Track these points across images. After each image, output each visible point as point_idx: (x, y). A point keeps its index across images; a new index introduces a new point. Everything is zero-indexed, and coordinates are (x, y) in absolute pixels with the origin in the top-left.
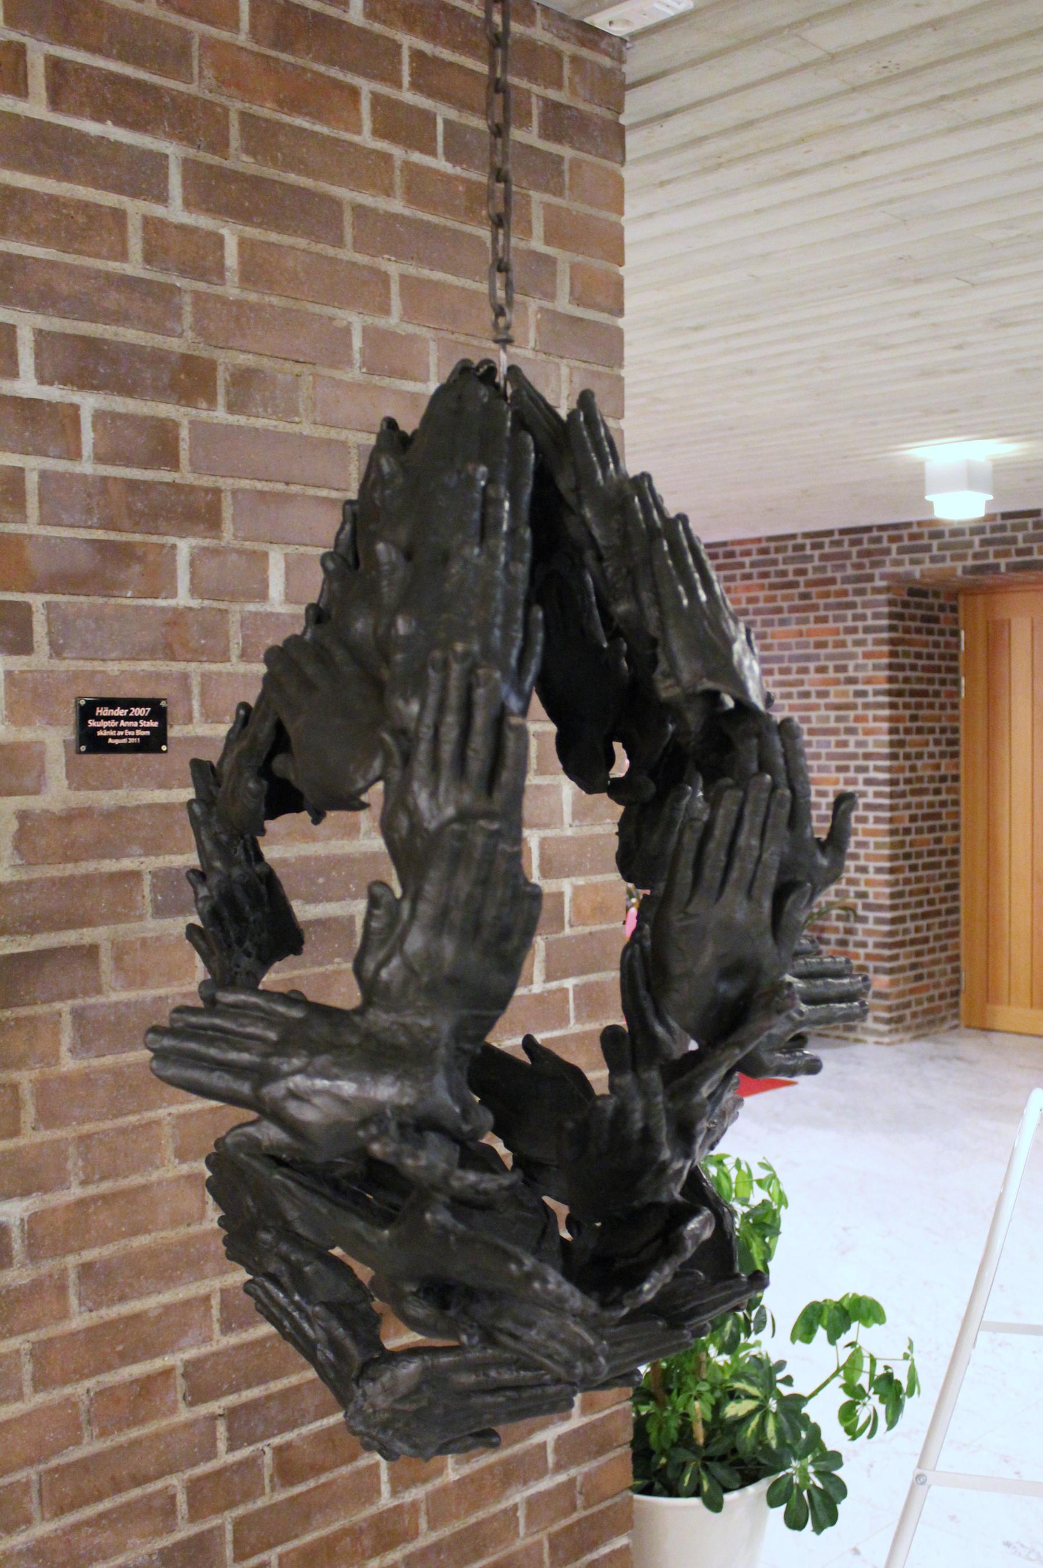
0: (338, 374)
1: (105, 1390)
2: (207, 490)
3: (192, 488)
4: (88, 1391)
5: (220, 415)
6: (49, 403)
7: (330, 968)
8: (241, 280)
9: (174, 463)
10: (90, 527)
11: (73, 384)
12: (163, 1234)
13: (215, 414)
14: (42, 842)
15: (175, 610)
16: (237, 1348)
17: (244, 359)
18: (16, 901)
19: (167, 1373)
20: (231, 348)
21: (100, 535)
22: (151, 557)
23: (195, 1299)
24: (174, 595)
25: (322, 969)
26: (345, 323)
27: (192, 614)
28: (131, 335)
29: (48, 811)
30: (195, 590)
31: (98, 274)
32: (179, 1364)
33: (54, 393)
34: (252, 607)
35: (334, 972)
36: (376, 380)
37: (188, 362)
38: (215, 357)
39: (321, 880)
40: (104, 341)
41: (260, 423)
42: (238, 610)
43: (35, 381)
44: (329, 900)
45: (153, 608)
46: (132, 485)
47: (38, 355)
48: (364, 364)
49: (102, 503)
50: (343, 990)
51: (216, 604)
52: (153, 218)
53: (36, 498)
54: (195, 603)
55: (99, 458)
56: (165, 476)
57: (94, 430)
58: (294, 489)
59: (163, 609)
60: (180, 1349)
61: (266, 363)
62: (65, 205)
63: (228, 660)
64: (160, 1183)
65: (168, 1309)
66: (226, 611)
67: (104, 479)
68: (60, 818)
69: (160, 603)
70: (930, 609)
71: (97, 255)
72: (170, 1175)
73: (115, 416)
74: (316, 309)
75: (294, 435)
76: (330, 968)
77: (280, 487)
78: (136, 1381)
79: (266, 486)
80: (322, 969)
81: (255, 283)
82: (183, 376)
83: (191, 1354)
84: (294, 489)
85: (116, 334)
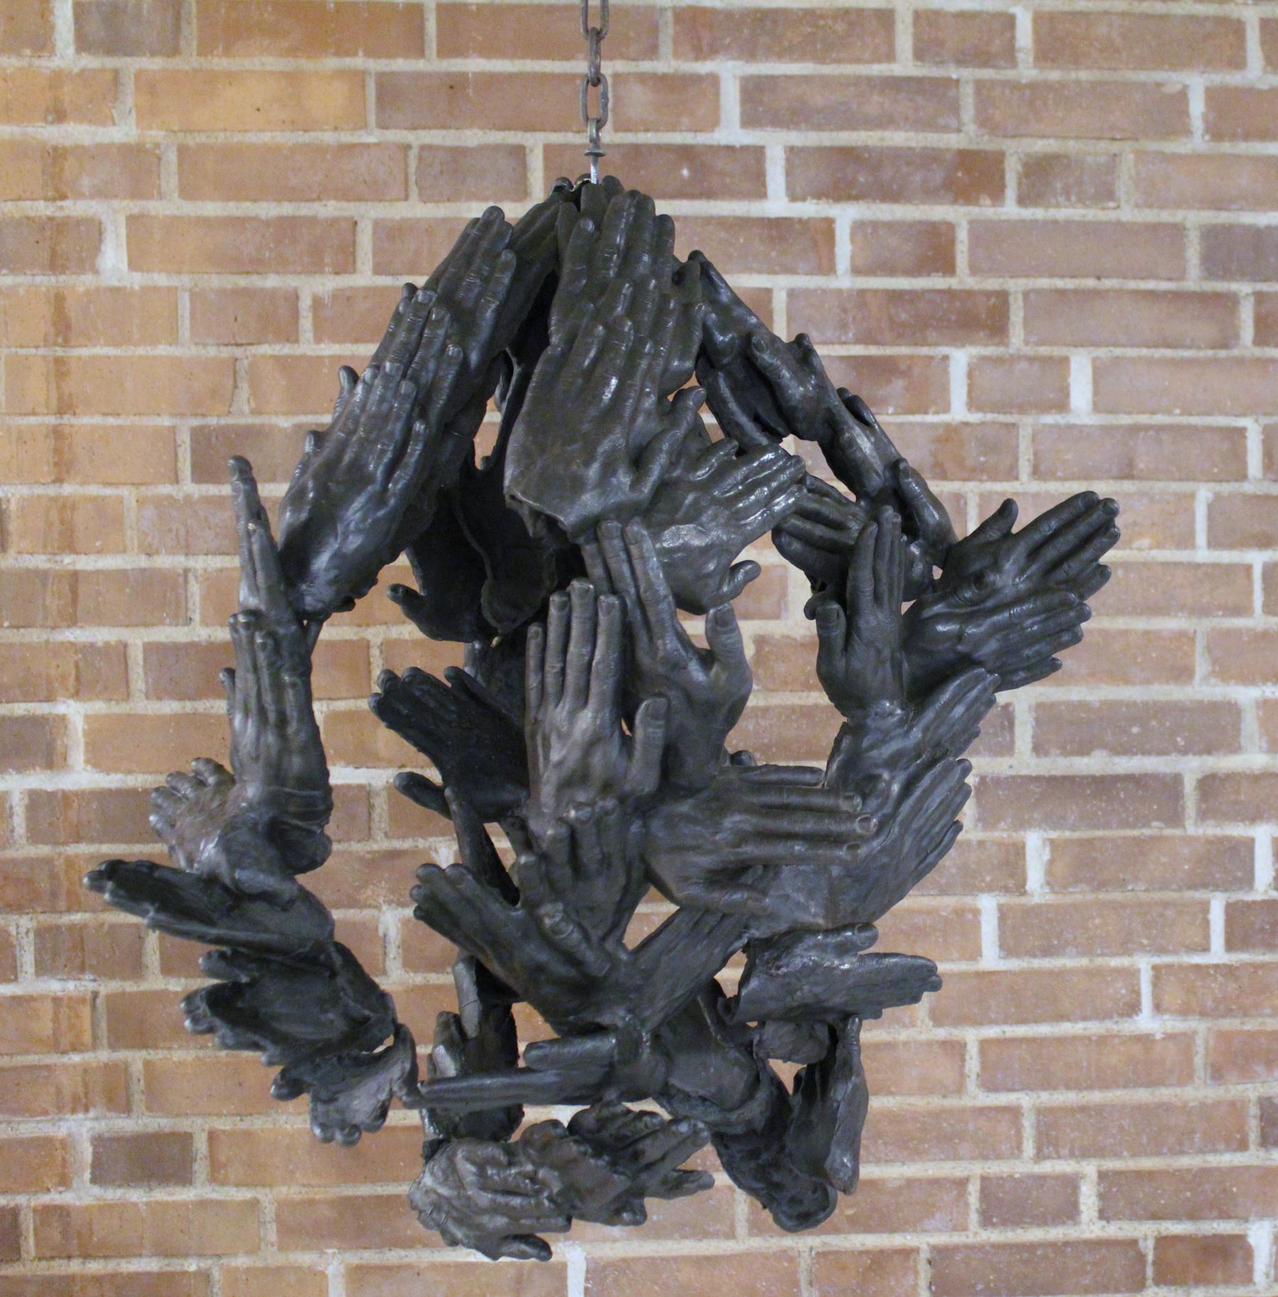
0: (1171, 147)
1: (830, 1253)
2: (988, 294)
3: (970, 293)
4: (811, 1249)
5: (1010, 209)
6: (800, 221)
7: (1147, 832)
8: (1037, 59)
9: (948, 267)
10: (845, 343)
11: (827, 197)
12: (912, 1100)
13: (1004, 210)
14: (781, 668)
15: (948, 426)
16: (998, 1247)
17: (1040, 146)
18: (751, 727)
19: (907, 1253)
20: (1022, 136)
21: (858, 350)
22: (916, 371)
23: (946, 1179)
24: (946, 409)
25: (1136, 833)
26: (1179, 87)
27: (967, 430)
28: (898, 138)
29: (788, 637)
30: (974, 403)
31: (857, 81)
32: (924, 1247)
33: (809, 209)
34: (1049, 419)
35: (1152, 838)
36: (1226, 147)
37: (966, 158)
38: (1004, 147)
39: (1135, 730)
40: (866, 148)
41: (1064, 213)
42: (1027, 423)
43: (786, 199)
44: (1146, 752)
45: (922, 425)
46: (895, 296)
47: (789, 173)
48: (1208, 130)
49: (859, 316)
50: (1164, 860)
51: (1002, 418)
52: (926, 11)
53: (785, 318)
54: (975, 418)
55: (856, 271)
56: (938, 282)
57: (852, 241)
58: (1108, 283)
59: (933, 426)
60: (924, 1231)
61: (1072, 146)
62: (822, 17)
63: (1017, 478)
64: (906, 1044)
65: (910, 1183)
66: (1014, 425)
67: (862, 293)
68: (803, 645)
69: (931, 418)
70: (1189, 1294)
71: (859, 61)
72: (923, 1037)
73: (875, 225)
74: (1142, 76)
75: (1108, 223)
76: (1147, 832)
77: (1090, 283)
78: (867, 1252)
79: (1069, 284)
80: (1136, 833)
81: (1053, 61)
82: (960, 174)
83: (942, 1239)
84: (1108, 283)
85: (882, 139)
